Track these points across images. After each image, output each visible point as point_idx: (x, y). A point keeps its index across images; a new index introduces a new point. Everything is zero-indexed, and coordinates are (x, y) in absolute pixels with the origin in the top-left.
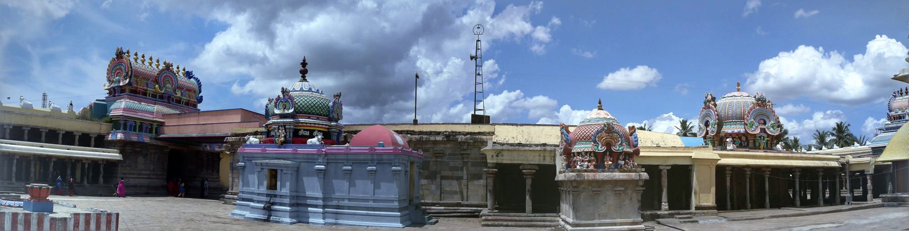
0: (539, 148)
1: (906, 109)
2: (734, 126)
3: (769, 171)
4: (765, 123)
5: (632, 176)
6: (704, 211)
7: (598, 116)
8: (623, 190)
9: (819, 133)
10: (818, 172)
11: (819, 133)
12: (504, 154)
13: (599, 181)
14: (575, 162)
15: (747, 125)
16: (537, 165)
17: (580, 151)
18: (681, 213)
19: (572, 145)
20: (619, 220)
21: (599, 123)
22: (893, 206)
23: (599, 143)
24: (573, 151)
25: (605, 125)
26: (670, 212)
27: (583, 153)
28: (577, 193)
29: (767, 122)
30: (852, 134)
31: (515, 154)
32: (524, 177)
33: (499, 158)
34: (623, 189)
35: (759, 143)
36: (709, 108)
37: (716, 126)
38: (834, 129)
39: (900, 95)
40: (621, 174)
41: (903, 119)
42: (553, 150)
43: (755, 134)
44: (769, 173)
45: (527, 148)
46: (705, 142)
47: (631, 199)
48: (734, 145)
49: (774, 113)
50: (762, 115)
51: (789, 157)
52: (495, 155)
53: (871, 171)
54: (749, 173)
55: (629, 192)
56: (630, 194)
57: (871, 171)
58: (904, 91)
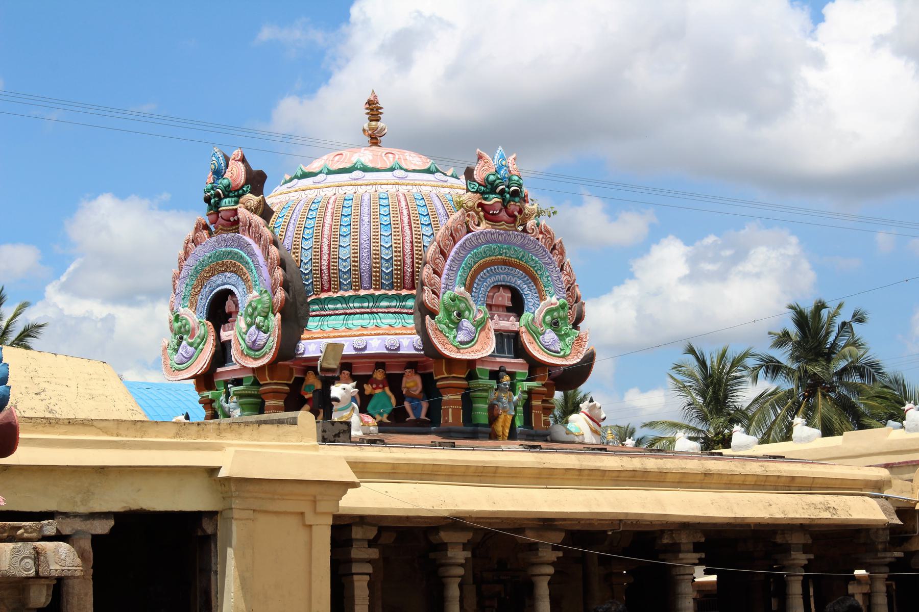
2: (366, 320)
4: (517, 307)
9: (702, 363)
10: (786, 549)
11: (702, 363)
15: (433, 314)
29: (529, 297)
30: (874, 366)
35: (492, 408)
36: (233, 224)
37: (275, 320)
38: (783, 339)
43: (471, 363)
44: (553, 556)
46: (208, 404)
48: (368, 419)
49: (562, 253)
50: (505, 263)
54: (552, 556)
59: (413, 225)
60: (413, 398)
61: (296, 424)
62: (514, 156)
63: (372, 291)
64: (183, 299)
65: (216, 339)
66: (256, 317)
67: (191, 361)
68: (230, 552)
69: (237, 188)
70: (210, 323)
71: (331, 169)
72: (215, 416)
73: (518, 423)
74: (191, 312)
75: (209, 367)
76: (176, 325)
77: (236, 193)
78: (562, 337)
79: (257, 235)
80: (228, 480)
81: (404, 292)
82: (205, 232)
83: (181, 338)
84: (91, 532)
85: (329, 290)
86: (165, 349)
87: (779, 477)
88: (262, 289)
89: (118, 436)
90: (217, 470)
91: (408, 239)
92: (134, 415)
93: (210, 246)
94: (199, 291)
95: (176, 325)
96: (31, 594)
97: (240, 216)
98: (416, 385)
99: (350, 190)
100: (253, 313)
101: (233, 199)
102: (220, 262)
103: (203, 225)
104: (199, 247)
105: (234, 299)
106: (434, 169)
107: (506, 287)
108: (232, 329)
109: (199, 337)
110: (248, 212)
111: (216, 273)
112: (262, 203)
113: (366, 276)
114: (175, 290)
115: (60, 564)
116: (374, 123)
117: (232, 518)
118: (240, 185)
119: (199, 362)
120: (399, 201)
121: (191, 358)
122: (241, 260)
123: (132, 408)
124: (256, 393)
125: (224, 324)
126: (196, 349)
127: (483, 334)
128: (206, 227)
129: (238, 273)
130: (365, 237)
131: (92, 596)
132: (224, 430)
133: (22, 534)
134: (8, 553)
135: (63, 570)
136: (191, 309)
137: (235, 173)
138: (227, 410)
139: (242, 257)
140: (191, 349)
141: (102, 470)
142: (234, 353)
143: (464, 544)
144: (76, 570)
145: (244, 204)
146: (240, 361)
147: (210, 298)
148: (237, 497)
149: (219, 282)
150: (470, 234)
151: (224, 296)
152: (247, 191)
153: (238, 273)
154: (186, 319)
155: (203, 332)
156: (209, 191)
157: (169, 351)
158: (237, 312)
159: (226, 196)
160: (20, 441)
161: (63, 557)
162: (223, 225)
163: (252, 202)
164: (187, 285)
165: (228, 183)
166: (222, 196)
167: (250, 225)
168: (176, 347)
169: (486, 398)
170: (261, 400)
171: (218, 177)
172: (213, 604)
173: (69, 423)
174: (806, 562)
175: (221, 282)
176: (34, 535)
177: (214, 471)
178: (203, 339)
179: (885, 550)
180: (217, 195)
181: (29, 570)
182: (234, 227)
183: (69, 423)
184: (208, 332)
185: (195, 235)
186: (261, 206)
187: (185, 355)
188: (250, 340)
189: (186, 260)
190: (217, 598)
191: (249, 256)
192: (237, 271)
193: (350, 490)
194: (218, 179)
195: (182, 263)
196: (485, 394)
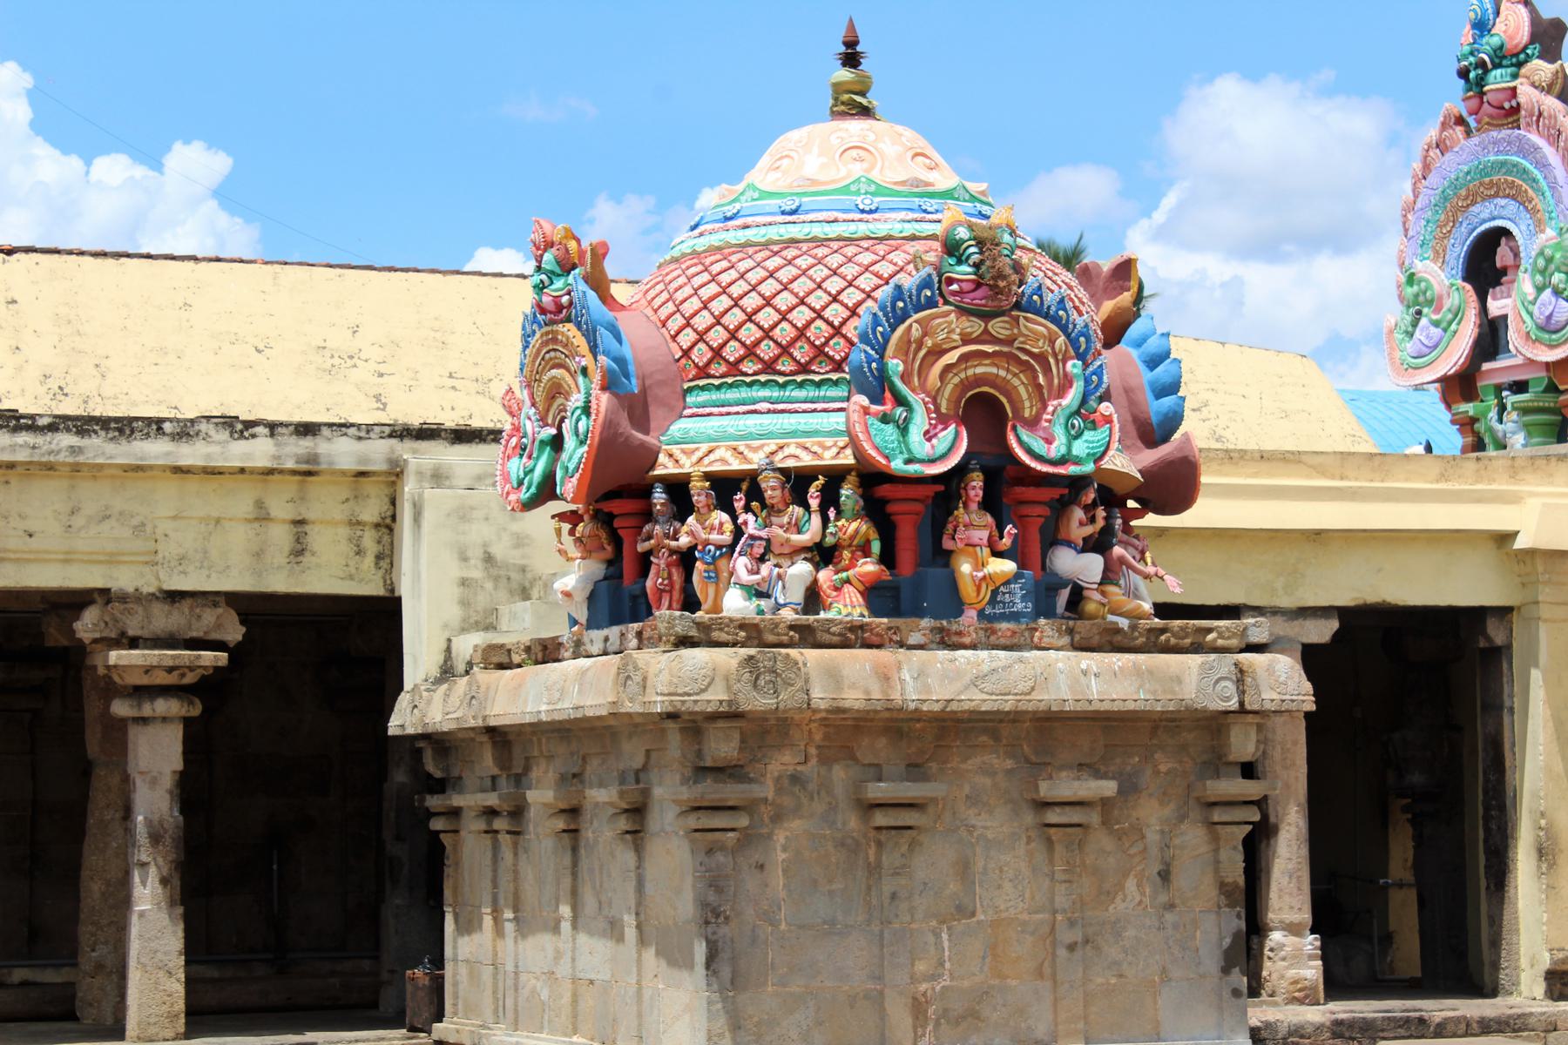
0: (259, 452)
5: (1179, 680)
7: (857, 170)
8: (1105, 803)
13: (917, 716)
14: (686, 559)
16: (235, 600)
17: (736, 465)
18: (1438, 1017)
19: (656, 413)
21: (881, 229)
23: (916, 400)
24: (665, 467)
25: (952, 248)
26: (1343, 1009)
27: (771, 486)
28: (743, 821)
32: (121, 708)
34: (1109, 787)
36: (1510, 113)
40: (1088, 660)
42: (379, 466)
45: (155, 450)
46: (1467, 425)
47: (1165, 876)
55: (1152, 814)
56: (1152, 836)
64: (1421, 246)
65: (1480, 313)
66: (1552, 274)
67: (1436, 351)
68: (1536, 675)
69: (1515, 51)
70: (1468, 287)
72: (1479, 446)
74: (1436, 268)
75: (1468, 363)
76: (1410, 291)
77: (1514, 60)
79: (1553, 132)
80: (1531, 553)
82: (1459, 130)
83: (1419, 313)
84: (1300, 639)
86: (1391, 332)
88: (1562, 225)
89: (1342, 479)
90: (1512, 536)
92: (1356, 445)
93: (1467, 153)
94: (1450, 232)
95: (1410, 291)
96: (1232, 739)
97: (1522, 99)
100: (1546, 268)
101: (1509, 70)
102: (1487, 180)
103: (1455, 117)
104: (1448, 156)
105: (1512, 244)
108: (1509, 296)
109: (1449, 310)
110: (1536, 92)
111: (1479, 199)
112: (1560, 75)
114: (1406, 230)
115: (1278, 690)
117: (1539, 618)
118: (1521, 46)
119: (1451, 355)
121: (1436, 346)
122: (1525, 176)
123: (1353, 432)
124: (1552, 405)
125: (1494, 287)
126: (1445, 330)
128: (1460, 121)
129: (1519, 199)
131: (1305, 746)
132: (1523, 468)
133: (1215, 640)
134: (1195, 671)
135: (1283, 701)
136: (1435, 263)
137: (1512, 24)
138: (1500, 435)
139: (1525, 171)
140: (1436, 332)
141: (1317, 537)
142: (1513, 337)
144: (1303, 701)
145: (1528, 78)
146: (1523, 351)
147: (1468, 242)
148: (1545, 583)
149: (1485, 215)
151: (1494, 238)
152: (1533, 54)
153: (1519, 199)
154: (1426, 281)
155: (1456, 302)
156: (1465, 57)
157: (1399, 336)
158: (1517, 267)
159: (1496, 66)
160: (1202, 489)
161: (1282, 679)
162: (1491, 116)
163: (1542, 73)
164: (1428, 222)
165: (1500, 43)
166: (1490, 66)
167: (1540, 114)
168: (1410, 329)
170: (1560, 418)
171: (1482, 32)
172: (1508, 764)
173: (1262, 457)
175: (1486, 215)
176: (1234, 642)
177: (1505, 538)
178: (1457, 313)
180: (1481, 64)
181: (1228, 699)
182: (1510, 120)
183: (1262, 457)
184: (1466, 302)
185: (1441, 135)
186: (1559, 81)
187: (1426, 342)
188: (1541, 313)
189: (1425, 178)
190: (1514, 754)
191: (1539, 169)
192: (1517, 196)
194: (1482, 36)
195: (1419, 185)
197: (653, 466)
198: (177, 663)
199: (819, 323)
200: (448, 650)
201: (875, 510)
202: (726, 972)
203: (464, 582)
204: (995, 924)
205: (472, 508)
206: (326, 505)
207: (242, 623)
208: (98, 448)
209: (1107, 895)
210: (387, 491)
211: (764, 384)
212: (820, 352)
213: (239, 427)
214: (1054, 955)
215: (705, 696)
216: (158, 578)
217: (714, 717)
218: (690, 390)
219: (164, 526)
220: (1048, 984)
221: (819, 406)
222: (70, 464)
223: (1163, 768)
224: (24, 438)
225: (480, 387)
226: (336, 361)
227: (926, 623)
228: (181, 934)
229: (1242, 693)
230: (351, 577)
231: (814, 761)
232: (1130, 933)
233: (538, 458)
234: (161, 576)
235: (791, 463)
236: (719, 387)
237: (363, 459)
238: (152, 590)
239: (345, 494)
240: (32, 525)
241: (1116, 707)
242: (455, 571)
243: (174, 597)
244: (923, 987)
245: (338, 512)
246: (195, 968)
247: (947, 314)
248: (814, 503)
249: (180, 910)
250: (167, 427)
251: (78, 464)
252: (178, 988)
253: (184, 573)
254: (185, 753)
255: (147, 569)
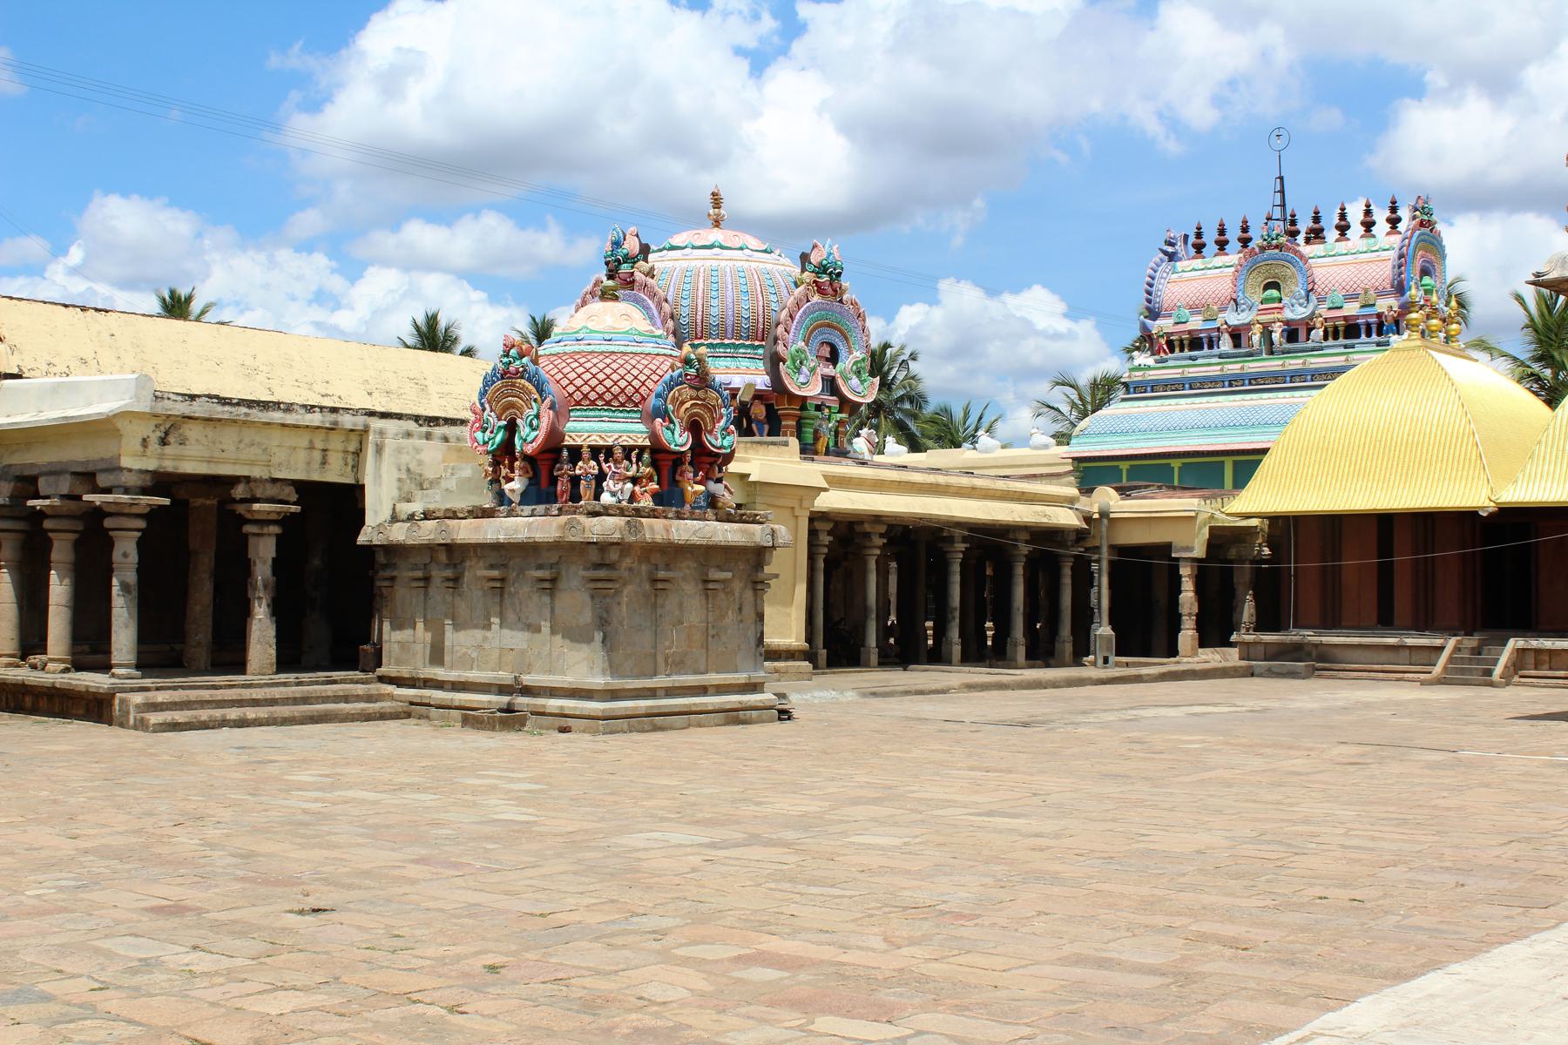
0: (315, 419)
1: (1223, 310)
3: (882, 536)
4: (833, 358)
6: (776, 664)
10: (950, 540)
12: (188, 433)
17: (601, 443)
20: (714, 678)
22: (1292, 674)
23: (676, 420)
27: (618, 453)
31: (228, 438)
32: (248, 529)
33: (168, 450)
35: (816, 432)
39: (1192, 251)
40: (727, 526)
41: (1206, 351)
43: (804, 398)
45: (277, 416)
47: (740, 609)
49: (864, 320)
50: (829, 326)
51: (938, 485)
52: (154, 438)
53: (1196, 546)
54: (880, 542)
57: (1199, 551)
58: (1210, 237)
59: (764, 294)
60: (759, 422)
61: (788, 446)
62: (837, 246)
63: (733, 341)
71: (694, 244)
73: (831, 444)
78: (862, 382)
80: (755, 483)
81: (757, 343)
85: (701, 338)
87: (1023, 493)
91: (761, 304)
98: (762, 412)
99: (715, 264)
106: (769, 251)
107: (828, 343)
113: (730, 330)
116: (716, 210)
120: (753, 274)
127: (814, 377)
130: (730, 300)
143: (828, 531)
148: (759, 495)
150: (809, 303)
159: (624, 262)
169: (812, 424)
174: (1027, 553)
179: (1072, 546)
181: (769, 542)
193: (822, 493)
196: (812, 422)
197: (563, 441)
198: (282, 510)
199: (630, 387)
200: (394, 509)
201: (654, 464)
202: (609, 645)
203: (400, 480)
204: (690, 627)
205: (403, 448)
206: (336, 443)
207: (297, 492)
208: (257, 415)
209: (723, 617)
210: (359, 438)
211: (606, 410)
212: (630, 399)
213: (309, 407)
214: (707, 640)
215: (613, 536)
216: (270, 473)
217: (613, 544)
218: (572, 410)
219: (276, 450)
220: (704, 651)
221: (629, 420)
222: (243, 421)
223: (741, 568)
224: (227, 408)
225: (309, 387)
226: (250, 371)
227: (674, 509)
228: (275, 629)
229: (773, 540)
230: (342, 475)
231: (636, 563)
232: (729, 631)
233: (497, 434)
234: (272, 472)
235: (625, 443)
236: (585, 410)
237: (355, 425)
238: (267, 477)
239: (343, 438)
240: (224, 447)
241: (736, 544)
242: (396, 475)
243: (275, 481)
244: (667, 651)
245: (340, 447)
246: (1397, 622)
247: (686, 388)
248: (634, 460)
249: (274, 618)
250: (282, 406)
251: (247, 421)
252: (273, 652)
253: (280, 470)
254: (277, 551)
255: (265, 468)
